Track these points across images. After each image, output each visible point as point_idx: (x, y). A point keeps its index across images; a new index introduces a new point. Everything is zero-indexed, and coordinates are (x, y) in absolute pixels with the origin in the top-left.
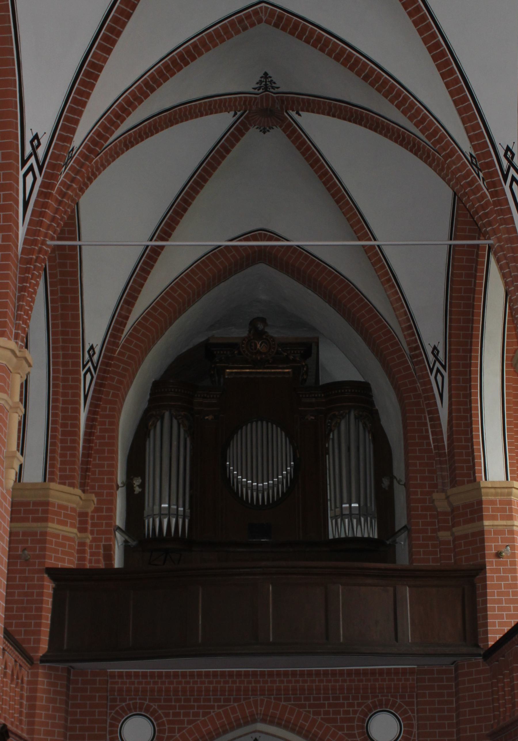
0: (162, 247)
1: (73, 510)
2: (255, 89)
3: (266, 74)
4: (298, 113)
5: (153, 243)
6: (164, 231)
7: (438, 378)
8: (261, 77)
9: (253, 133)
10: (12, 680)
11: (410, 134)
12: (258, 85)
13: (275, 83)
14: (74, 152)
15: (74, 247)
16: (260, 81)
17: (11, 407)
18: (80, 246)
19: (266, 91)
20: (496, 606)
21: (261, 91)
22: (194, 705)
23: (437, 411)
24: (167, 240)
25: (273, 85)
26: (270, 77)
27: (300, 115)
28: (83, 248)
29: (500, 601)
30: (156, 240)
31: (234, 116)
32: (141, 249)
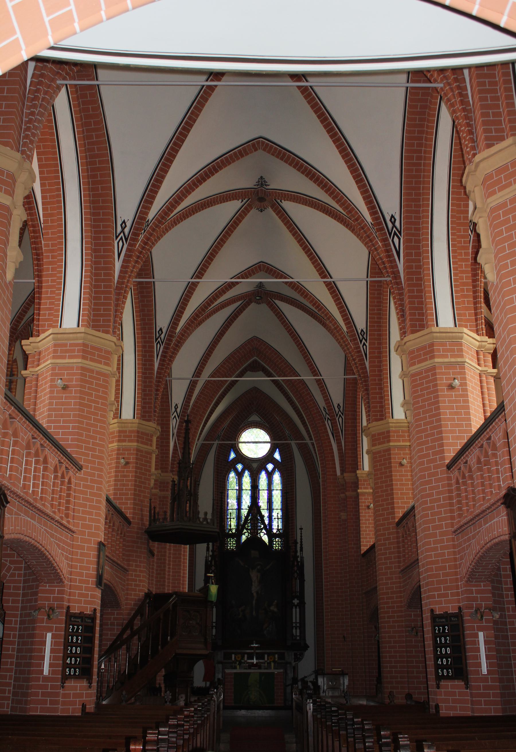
0: (198, 283)
1: (130, 432)
2: (255, 185)
3: (261, 177)
4: (281, 201)
5: (193, 280)
6: (200, 273)
7: (394, 240)
8: (259, 179)
9: (254, 212)
10: (118, 534)
11: (354, 157)
12: (257, 183)
13: (267, 182)
14: (149, 223)
15: (150, 283)
16: (259, 181)
17: (112, 374)
18: (154, 282)
19: (262, 187)
20: (81, 496)
21: (259, 186)
22: (139, 592)
23: (397, 266)
24: (201, 278)
25: (266, 183)
26: (264, 179)
27: (282, 202)
28: (156, 283)
29: (366, 524)
30: (194, 279)
31: (241, 202)
32: (186, 284)
